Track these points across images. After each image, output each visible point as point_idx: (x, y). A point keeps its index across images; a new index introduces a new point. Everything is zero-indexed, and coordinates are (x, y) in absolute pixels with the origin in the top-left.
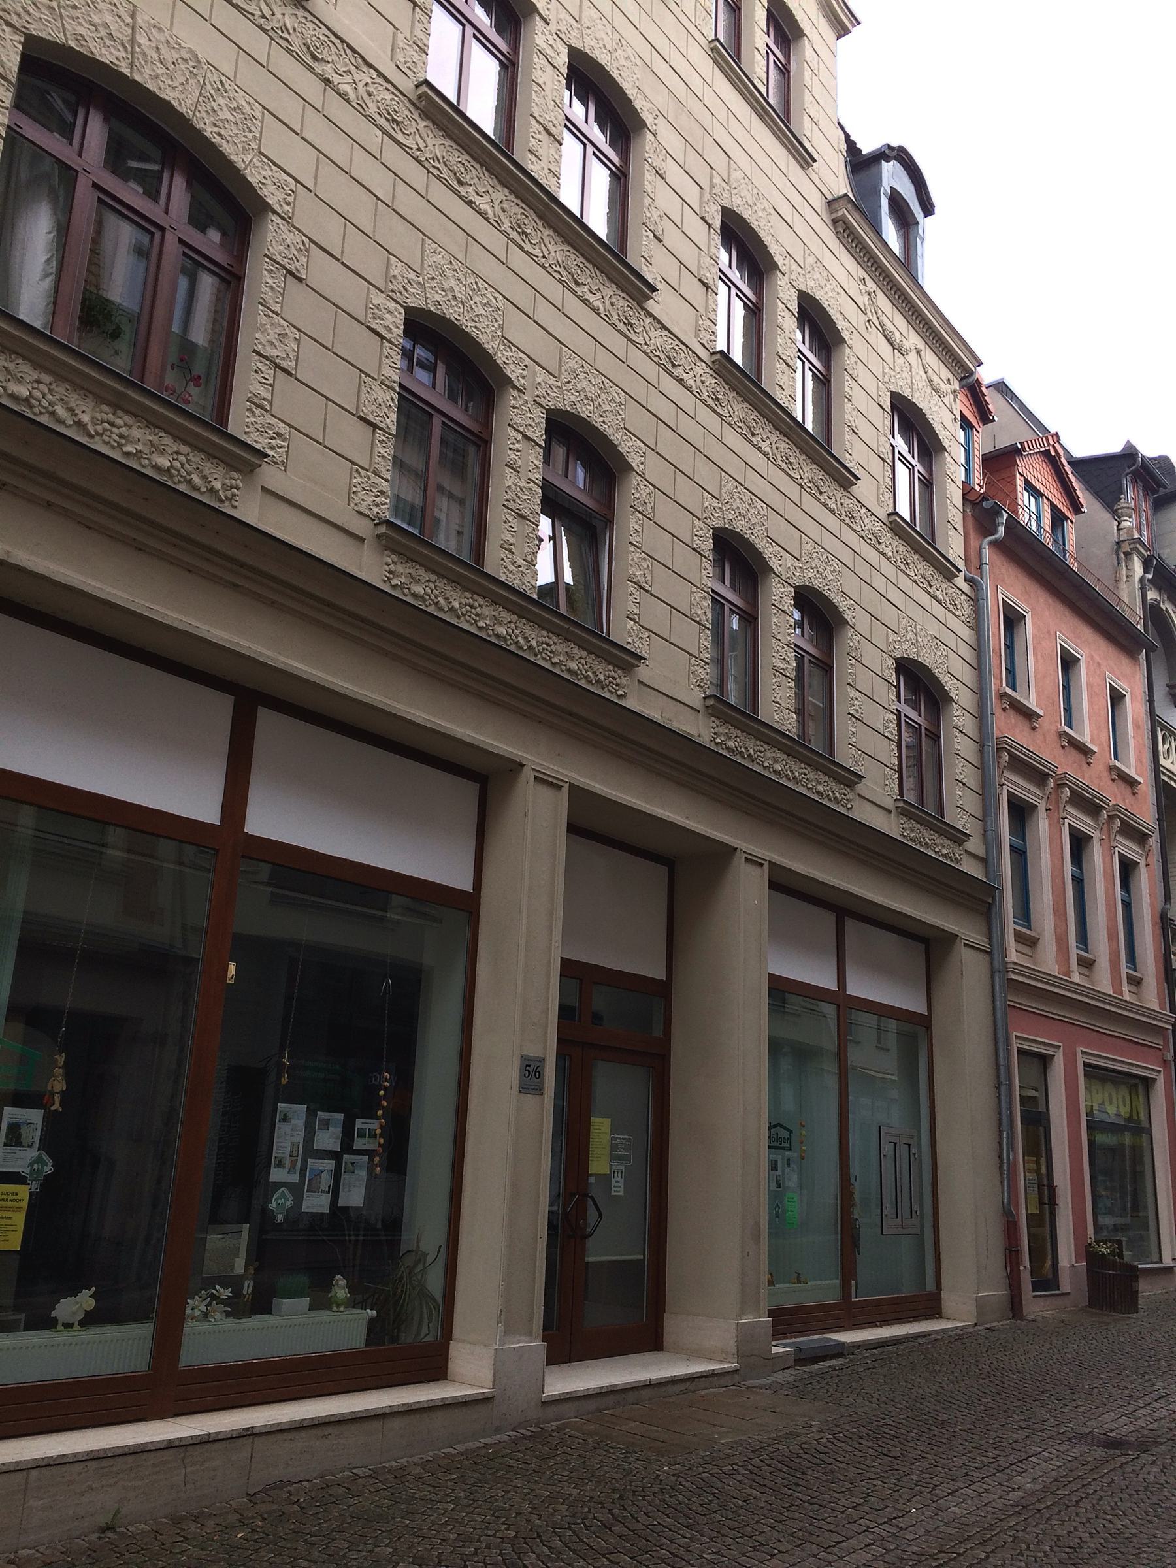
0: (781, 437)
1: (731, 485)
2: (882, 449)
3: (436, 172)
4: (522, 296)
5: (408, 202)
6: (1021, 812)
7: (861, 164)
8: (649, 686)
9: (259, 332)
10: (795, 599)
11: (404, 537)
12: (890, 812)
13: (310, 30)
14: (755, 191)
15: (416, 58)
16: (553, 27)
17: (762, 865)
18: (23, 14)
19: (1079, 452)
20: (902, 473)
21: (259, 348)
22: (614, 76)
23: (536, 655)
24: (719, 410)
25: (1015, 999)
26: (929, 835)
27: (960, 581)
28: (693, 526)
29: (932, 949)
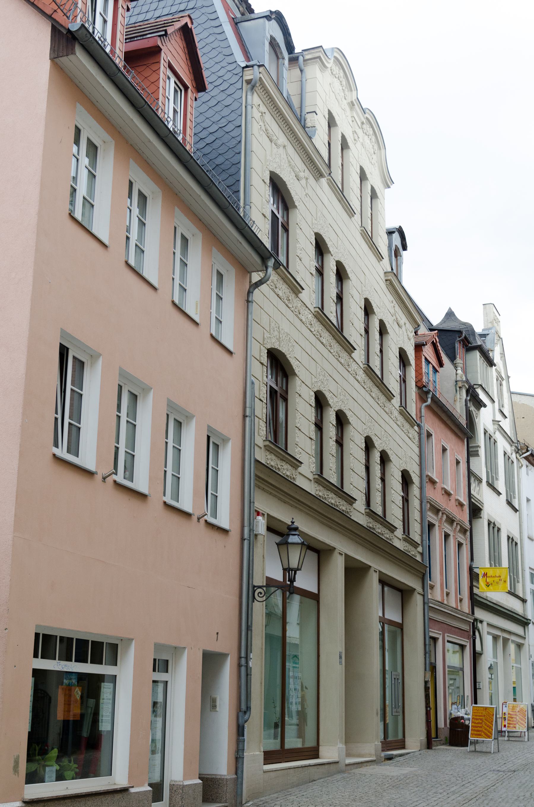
12: (400, 540)
25: (432, 615)
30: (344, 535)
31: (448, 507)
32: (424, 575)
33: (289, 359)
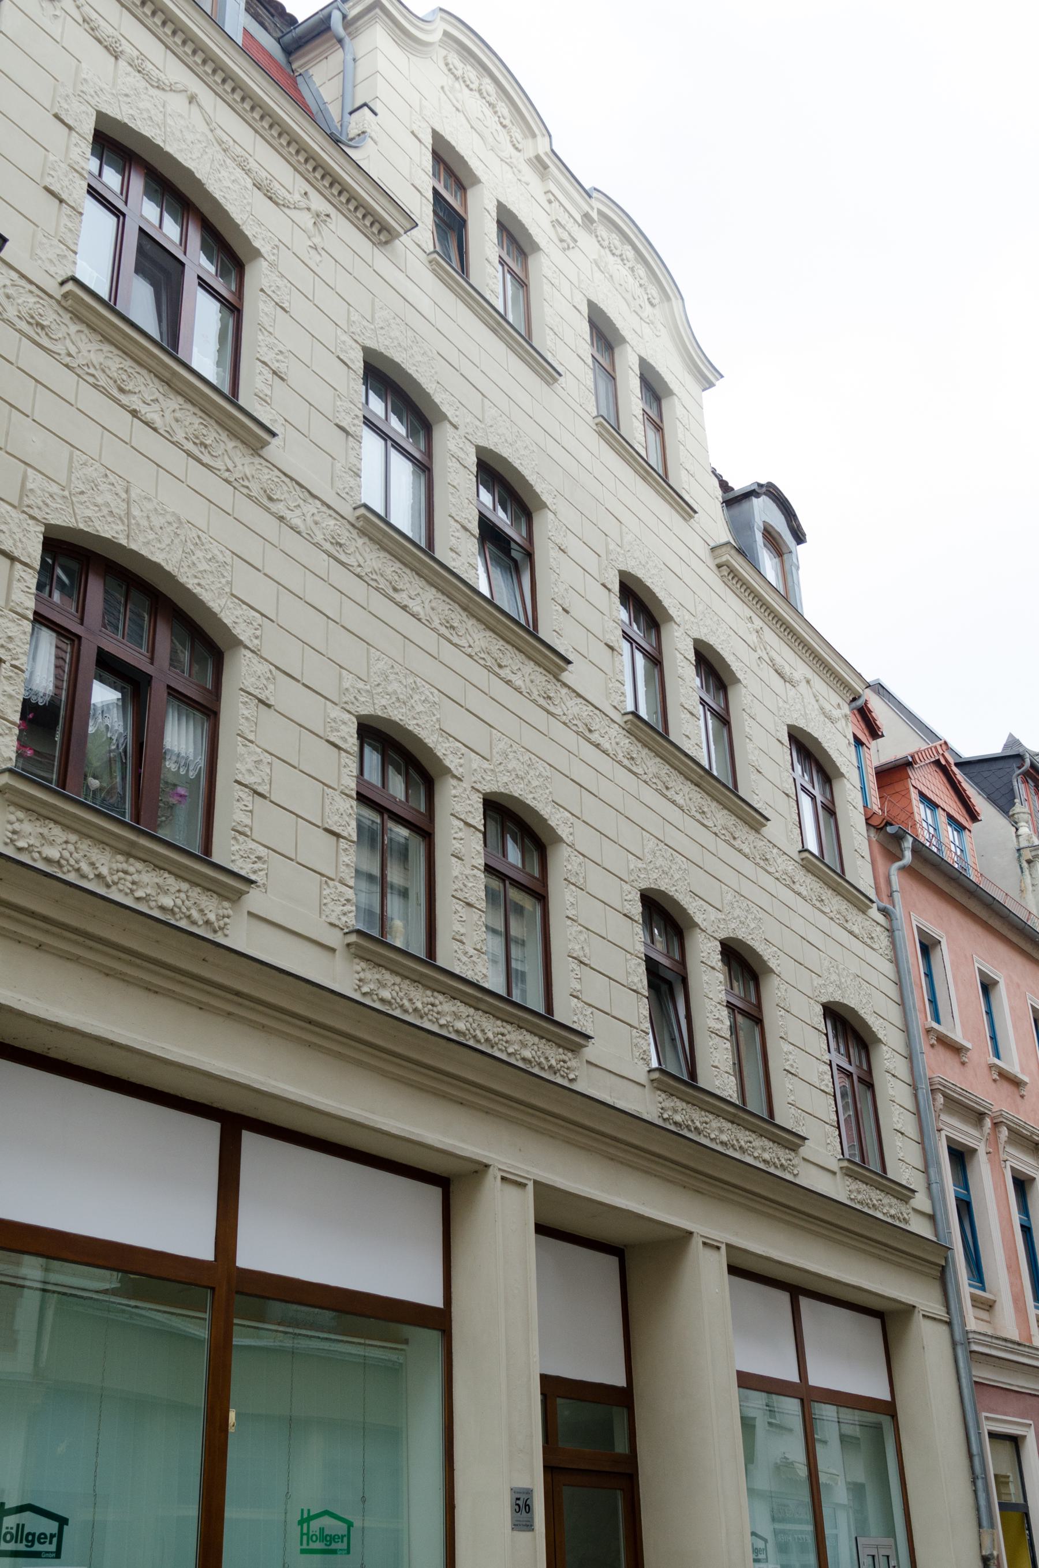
0: (693, 787)
1: (652, 843)
2: (785, 785)
3: (374, 584)
4: (453, 686)
5: (354, 618)
6: (960, 1156)
7: (734, 500)
8: (596, 1066)
9: (237, 762)
10: (722, 953)
11: (371, 944)
12: (834, 1173)
13: (267, 476)
14: (646, 551)
15: (352, 483)
16: (462, 431)
17: (718, 1248)
18: (43, 507)
19: (968, 752)
20: (806, 802)
21: (239, 778)
22: (516, 465)
23: (493, 1047)
24: (634, 769)
25: (985, 1374)
26: (875, 1195)
27: (874, 912)
28: (622, 891)
29: (888, 1321)
30: (647, 1172)
31: (1018, 1112)
32: (943, 1270)
33: (864, 1016)
